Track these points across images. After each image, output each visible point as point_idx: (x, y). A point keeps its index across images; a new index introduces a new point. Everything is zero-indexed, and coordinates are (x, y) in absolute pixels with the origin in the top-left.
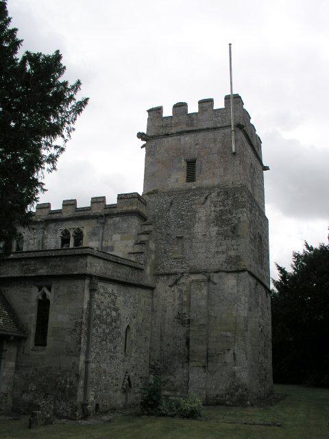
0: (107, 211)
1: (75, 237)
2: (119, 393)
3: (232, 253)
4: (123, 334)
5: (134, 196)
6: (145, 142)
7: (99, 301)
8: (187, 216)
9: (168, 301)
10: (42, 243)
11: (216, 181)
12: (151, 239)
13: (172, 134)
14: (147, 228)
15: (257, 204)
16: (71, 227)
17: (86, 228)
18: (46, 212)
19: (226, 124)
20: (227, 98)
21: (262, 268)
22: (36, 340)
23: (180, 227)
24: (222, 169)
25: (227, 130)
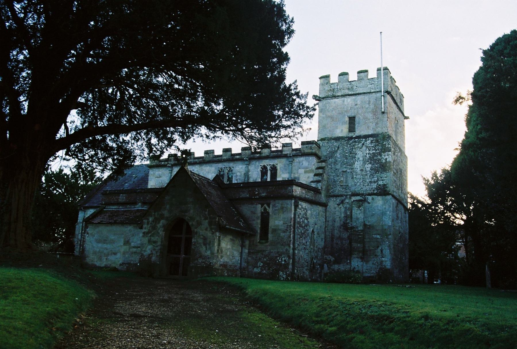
1: (271, 171)
3: (381, 183)
6: (317, 102)
7: (299, 213)
8: (350, 156)
9: (337, 214)
10: (247, 175)
13: (338, 96)
14: (320, 165)
15: (400, 148)
17: (280, 164)
18: (229, 153)
19: (378, 90)
20: (379, 70)
21: (402, 193)
22: (260, 237)
23: (345, 164)
24: (374, 124)
25: (379, 95)
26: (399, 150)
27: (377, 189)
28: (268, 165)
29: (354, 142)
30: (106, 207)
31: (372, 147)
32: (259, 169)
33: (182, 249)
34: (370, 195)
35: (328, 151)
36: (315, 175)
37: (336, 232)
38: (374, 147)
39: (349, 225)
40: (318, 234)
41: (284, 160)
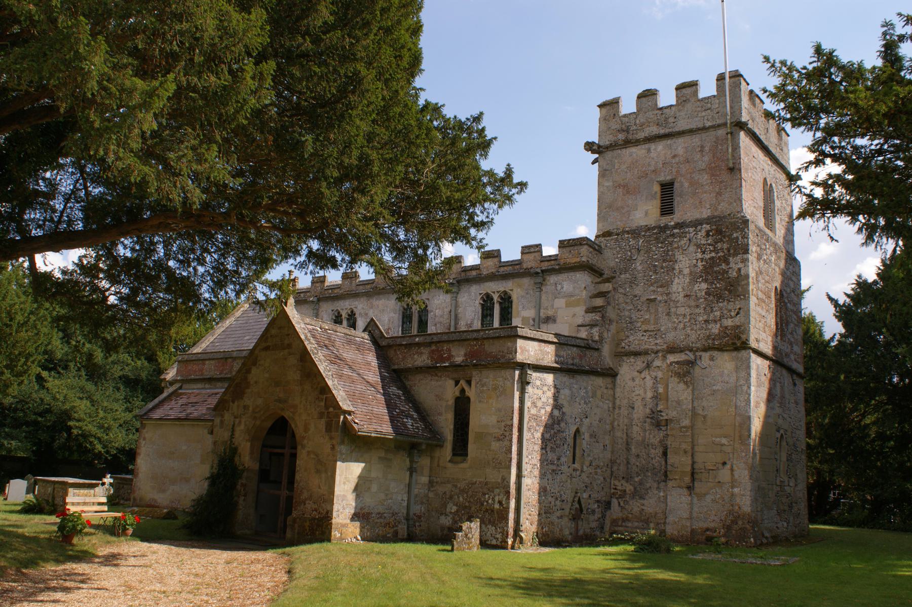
0: (545, 266)
1: (500, 303)
2: (566, 519)
3: (729, 323)
4: (570, 441)
5: (581, 242)
6: (596, 156)
8: (662, 268)
9: (637, 392)
11: (706, 213)
12: (609, 303)
16: (494, 288)
17: (518, 290)
19: (719, 122)
20: (721, 78)
22: (454, 449)
23: (652, 285)
25: (721, 132)
26: (771, 249)
27: (719, 336)
28: (494, 292)
29: (671, 235)
30: (184, 386)
31: (709, 245)
32: (477, 302)
33: (285, 481)
34: (705, 350)
35: (617, 258)
36: (589, 311)
37: (635, 429)
38: (712, 245)
39: (662, 416)
40: (593, 436)
41: (526, 281)
